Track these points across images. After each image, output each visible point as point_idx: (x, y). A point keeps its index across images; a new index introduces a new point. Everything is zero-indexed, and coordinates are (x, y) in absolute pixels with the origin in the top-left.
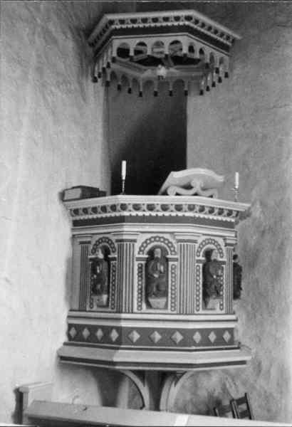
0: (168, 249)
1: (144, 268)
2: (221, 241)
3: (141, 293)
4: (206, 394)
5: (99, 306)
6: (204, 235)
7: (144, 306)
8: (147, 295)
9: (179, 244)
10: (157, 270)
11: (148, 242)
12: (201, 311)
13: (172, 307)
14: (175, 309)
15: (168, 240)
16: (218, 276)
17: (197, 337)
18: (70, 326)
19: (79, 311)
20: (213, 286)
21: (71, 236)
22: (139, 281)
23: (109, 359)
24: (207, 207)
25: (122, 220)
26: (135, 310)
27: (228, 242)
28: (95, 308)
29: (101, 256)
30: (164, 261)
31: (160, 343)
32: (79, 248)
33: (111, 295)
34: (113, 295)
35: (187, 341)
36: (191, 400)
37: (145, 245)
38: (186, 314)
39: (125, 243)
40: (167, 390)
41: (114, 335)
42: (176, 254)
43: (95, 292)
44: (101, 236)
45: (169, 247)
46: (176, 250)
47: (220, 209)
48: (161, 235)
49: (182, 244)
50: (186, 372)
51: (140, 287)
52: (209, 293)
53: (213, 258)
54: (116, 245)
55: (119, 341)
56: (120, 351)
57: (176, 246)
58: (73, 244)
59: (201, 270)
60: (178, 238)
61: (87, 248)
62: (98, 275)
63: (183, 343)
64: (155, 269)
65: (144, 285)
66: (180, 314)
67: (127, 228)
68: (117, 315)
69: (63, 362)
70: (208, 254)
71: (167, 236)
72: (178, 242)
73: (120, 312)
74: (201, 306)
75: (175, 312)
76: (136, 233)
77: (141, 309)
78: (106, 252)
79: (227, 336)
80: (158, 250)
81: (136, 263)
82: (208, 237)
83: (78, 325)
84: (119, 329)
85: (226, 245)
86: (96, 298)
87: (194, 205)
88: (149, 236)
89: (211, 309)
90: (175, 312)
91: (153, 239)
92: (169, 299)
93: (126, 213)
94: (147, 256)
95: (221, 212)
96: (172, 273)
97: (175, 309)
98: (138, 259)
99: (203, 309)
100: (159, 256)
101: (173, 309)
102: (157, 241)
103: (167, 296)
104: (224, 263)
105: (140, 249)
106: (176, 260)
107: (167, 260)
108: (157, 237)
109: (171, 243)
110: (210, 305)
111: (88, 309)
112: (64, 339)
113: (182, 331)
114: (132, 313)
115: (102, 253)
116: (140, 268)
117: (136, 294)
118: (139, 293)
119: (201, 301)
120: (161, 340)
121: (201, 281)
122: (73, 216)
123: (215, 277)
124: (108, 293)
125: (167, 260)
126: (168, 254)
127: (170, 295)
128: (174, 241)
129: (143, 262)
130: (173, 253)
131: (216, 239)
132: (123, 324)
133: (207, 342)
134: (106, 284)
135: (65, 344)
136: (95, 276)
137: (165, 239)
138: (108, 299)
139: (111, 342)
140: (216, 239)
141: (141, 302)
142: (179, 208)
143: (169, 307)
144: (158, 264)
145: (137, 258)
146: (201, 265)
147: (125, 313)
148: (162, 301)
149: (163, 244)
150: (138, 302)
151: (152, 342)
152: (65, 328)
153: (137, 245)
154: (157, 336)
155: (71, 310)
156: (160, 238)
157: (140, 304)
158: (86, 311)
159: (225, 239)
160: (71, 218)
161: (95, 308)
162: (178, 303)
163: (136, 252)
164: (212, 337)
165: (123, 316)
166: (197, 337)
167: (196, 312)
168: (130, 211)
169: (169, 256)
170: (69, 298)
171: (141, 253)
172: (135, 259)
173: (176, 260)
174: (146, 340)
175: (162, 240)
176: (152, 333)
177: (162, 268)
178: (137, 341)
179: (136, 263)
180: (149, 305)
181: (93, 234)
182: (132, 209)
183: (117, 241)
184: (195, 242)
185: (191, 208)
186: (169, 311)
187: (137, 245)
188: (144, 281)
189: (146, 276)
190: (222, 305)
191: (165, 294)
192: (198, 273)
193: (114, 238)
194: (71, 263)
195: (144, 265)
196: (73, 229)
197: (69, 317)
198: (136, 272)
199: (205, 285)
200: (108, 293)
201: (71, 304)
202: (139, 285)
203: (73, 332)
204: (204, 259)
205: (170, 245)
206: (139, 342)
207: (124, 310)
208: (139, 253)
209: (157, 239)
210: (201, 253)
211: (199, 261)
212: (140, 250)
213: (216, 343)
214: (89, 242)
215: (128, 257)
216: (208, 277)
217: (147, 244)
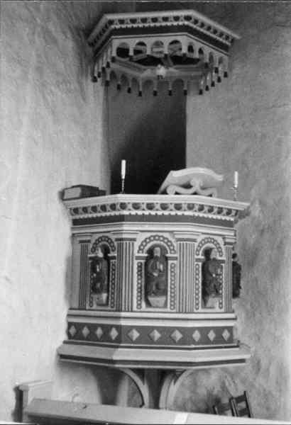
0: (167, 247)
1: (143, 267)
2: (220, 240)
3: (141, 292)
4: (205, 393)
5: (99, 305)
6: (203, 233)
7: (144, 304)
8: (147, 294)
9: (179, 242)
10: (156, 268)
11: (148, 240)
12: (200, 310)
13: (171, 305)
14: (174, 308)
15: (167, 239)
16: (217, 275)
17: (197, 335)
18: (70, 325)
19: (79, 309)
20: (212, 285)
21: (71, 235)
22: (138, 279)
23: (109, 358)
24: (206, 206)
25: (121, 219)
26: (135, 309)
27: (227, 240)
28: (95, 307)
29: (100, 255)
30: (164, 260)
31: (160, 341)
32: (79, 247)
33: (110, 293)
34: (113, 293)
35: (187, 339)
36: (191, 398)
37: (144, 244)
38: (186, 313)
39: (124, 242)
40: (167, 388)
41: (114, 333)
42: (175, 253)
43: (95, 290)
44: (101, 235)
45: (168, 246)
46: (175, 249)
47: (219, 208)
48: (160, 234)
49: (182, 242)
50: (185, 370)
51: (139, 286)
52: (208, 292)
53: (212, 257)
54: (116, 244)
55: (118, 340)
56: (120, 349)
57: (175, 244)
58: (73, 243)
59: (200, 269)
60: (177, 236)
61: (87, 247)
62: (98, 274)
63: (183, 341)
64: (155, 268)
65: (143, 284)
66: (179, 312)
67: (127, 227)
68: (117, 314)
69: (63, 360)
70: (207, 253)
71: (166, 235)
72: (177, 241)
73: (120, 310)
74: (200, 305)
75: (174, 311)
76: (136, 232)
77: (141, 307)
78: (106, 251)
80: (158, 249)
81: (136, 262)
82: (208, 236)
83: (78, 323)
84: (119, 328)
85: (225, 244)
86: (95, 296)
87: (193, 204)
88: (148, 235)
89: (210, 308)
90: (174, 311)
91: (152, 238)
92: (169, 297)
93: (125, 212)
94: (146, 255)
95: (220, 211)
96: (172, 272)
97: (174, 308)
98: (138, 258)
99: (202, 307)
100: (159, 255)
101: (172, 307)
102: (157, 240)
103: (167, 294)
104: (223, 262)
105: (139, 247)
106: (176, 259)
107: (167, 259)
108: (157, 236)
109: (170, 242)
110: (209, 304)
111: (87, 308)
112: (64, 337)
113: (181, 330)
114: (132, 311)
115: (102, 251)
116: (140, 267)
117: (135, 292)
118: (138, 292)
119: (200, 299)
120: (160, 338)
121: (200, 280)
122: (72, 215)
123: (214, 275)
124: (108, 291)
125: (167, 259)
126: (167, 253)
127: (169, 293)
128: (173, 240)
129: (143, 261)
130: (173, 252)
131: (216, 238)
132: (123, 323)
133: (207, 341)
134: (106, 283)
135: (65, 342)
136: (95, 275)
137: (164, 238)
138: (108, 298)
139: (111, 341)
140: (216, 238)
141: (140, 300)
142: (178, 207)
143: (169, 306)
144: (158, 263)
145: (136, 257)
146: (200, 264)
147: (125, 311)
148: (161, 300)
149: (162, 243)
150: (138, 300)
151: (151, 340)
152: (65, 326)
153: (137, 244)
154: (157, 335)
155: (71, 309)
156: (159, 237)
157: (139, 302)
158: (85, 309)
159: (224, 238)
160: (71, 217)
161: (95, 307)
162: (177, 302)
163: (136, 251)
164: (212, 335)
165: (123, 314)
166: (197, 335)
167: (195, 311)
168: (130, 210)
169: (168, 255)
170: (69, 297)
171: (141, 252)
172: (134, 258)
173: (176, 259)
174: (146, 338)
175: (161, 239)
176: (151, 332)
177: (161, 267)
178: (137, 339)
179: (136, 262)
180: (149, 304)
181: (93, 233)
182: (131, 208)
183: (117, 240)
184: (194, 240)
185: (191, 207)
186: (169, 310)
187: (137, 244)
188: (143, 279)
189: (146, 275)
190: (221, 303)
191: (165, 293)
192: (197, 272)
193: (113, 237)
194: (70, 261)
195: (143, 264)
196: (72, 228)
197: (69, 315)
198: (135, 270)
199: (204, 284)
200: (108, 291)
201: (70, 303)
202: (138, 283)
203: (73, 330)
204: (203, 257)
205: (169, 244)
206: (138, 341)
207: (123, 309)
208: (138, 252)
209: (157, 238)
210: (201, 252)
211: (198, 260)
212: (140, 249)
213: (216, 341)
214: (89, 241)
215: (128, 255)
216: (208, 275)
217: (147, 243)
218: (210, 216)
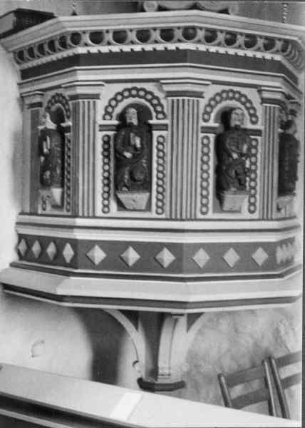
0: (152, 108)
1: (112, 143)
2: (252, 95)
4: (251, 342)
5: (55, 207)
6: (215, 82)
7: (113, 205)
8: (116, 188)
9: (170, 99)
10: (129, 143)
12: (210, 215)
13: (158, 207)
15: (151, 93)
16: (241, 155)
18: (21, 237)
19: (30, 214)
20: (233, 173)
21: (18, 95)
22: (105, 164)
23: (52, 292)
24: (222, 31)
25: (76, 60)
27: (266, 95)
28: (49, 210)
29: (51, 125)
30: (144, 129)
31: (137, 266)
32: (28, 113)
34: (69, 188)
35: (182, 266)
36: (229, 350)
37: (113, 103)
38: (182, 220)
41: (68, 252)
42: (165, 117)
43: (45, 184)
46: (165, 111)
47: (248, 36)
48: (139, 85)
49: (175, 98)
50: (199, 315)
52: (225, 186)
53: (234, 123)
55: (74, 264)
56: (73, 278)
57: (163, 102)
58: (22, 110)
59: (212, 146)
60: (166, 88)
61: (37, 112)
62: (46, 156)
63: (176, 266)
64: (127, 144)
65: (112, 171)
66: (171, 219)
67: (84, 75)
68: (69, 221)
69: (7, 291)
70: (225, 116)
71: (149, 87)
72: (167, 96)
73: (75, 216)
74: (210, 205)
80: (133, 111)
82: (129, 85)
83: (44, 237)
84: (75, 243)
85: (264, 101)
86: (44, 193)
87: (194, 28)
89: (231, 211)
90: (163, 216)
91: (243, 99)
92: (154, 193)
93: (81, 50)
94: (116, 122)
96: (159, 150)
98: (103, 128)
99: (214, 211)
100: (135, 122)
102: (134, 96)
103: (150, 190)
104: (258, 133)
106: (165, 127)
107: (151, 128)
108: (134, 88)
109: (157, 98)
110: (227, 205)
112: (13, 257)
113: (172, 247)
114: (94, 217)
115: (52, 120)
116: (106, 142)
118: (105, 185)
119: (211, 197)
120: (138, 261)
121: (211, 163)
122: (18, 63)
123: (235, 156)
124: (62, 186)
125: (151, 128)
127: (154, 187)
128: (161, 95)
129: (111, 133)
130: (161, 116)
131: (244, 91)
132: (80, 235)
134: (58, 171)
135: (13, 265)
136: (42, 159)
137: (147, 92)
138: (63, 193)
140: (244, 91)
141: (108, 199)
142: (167, 35)
143: (154, 207)
144: (132, 135)
145: (101, 126)
146: (212, 137)
147: (83, 217)
148: (141, 198)
149: (143, 101)
151: (124, 264)
152: (14, 239)
153: (101, 105)
154: (132, 256)
155: (22, 213)
156: (138, 90)
157: (106, 202)
159: (260, 91)
160: (18, 67)
162: (167, 201)
164: (98, 255)
165: (79, 222)
167: (199, 216)
169: (153, 121)
170: (17, 192)
173: (165, 127)
174: (115, 264)
177: (138, 142)
184: (200, 95)
185: (189, 34)
186: (154, 215)
187: (101, 105)
188: (112, 164)
189: (116, 157)
190: (251, 204)
191: (146, 186)
192: (206, 150)
194: (18, 138)
195: (112, 138)
196: (19, 84)
197: (18, 223)
198: (99, 149)
199: (218, 170)
201: (22, 204)
203: (23, 247)
204: (217, 125)
205: (155, 102)
206: (104, 265)
207: (81, 214)
208: (104, 119)
210: (213, 115)
211: (206, 130)
212: (107, 113)
216: (225, 156)
218: (250, 53)
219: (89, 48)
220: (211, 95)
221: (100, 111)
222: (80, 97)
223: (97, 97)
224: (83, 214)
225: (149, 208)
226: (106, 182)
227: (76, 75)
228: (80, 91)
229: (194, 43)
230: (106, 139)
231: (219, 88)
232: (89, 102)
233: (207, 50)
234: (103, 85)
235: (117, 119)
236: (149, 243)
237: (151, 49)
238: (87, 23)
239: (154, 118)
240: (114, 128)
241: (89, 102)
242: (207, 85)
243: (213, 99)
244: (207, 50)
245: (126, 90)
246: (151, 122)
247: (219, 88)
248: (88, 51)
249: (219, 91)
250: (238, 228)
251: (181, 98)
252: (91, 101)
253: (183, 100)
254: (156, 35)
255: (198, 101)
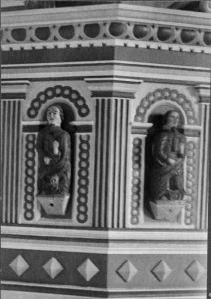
3: (138, 193)
6: (147, 80)
9: (95, 98)
10: (173, 150)
14: (191, 222)
26: (129, 225)
28: (38, 218)
33: (76, 195)
39: (113, 99)
44: (52, 84)
45: (182, 105)
48: (172, 87)
51: (136, 181)
54: (91, 103)
71: (182, 89)
75: (192, 227)
76: (135, 81)
77: (138, 222)
78: (67, 116)
79: (90, 270)
81: (131, 137)
82: (162, 86)
86: (46, 201)
90: (192, 227)
91: (50, 93)
94: (151, 125)
95: (163, 35)
97: (191, 222)
101: (188, 221)
102: (65, 96)
105: (138, 110)
106: (88, 129)
108: (167, 89)
111: (21, 220)
114: (125, 228)
116: (138, 146)
117: (129, 193)
123: (172, 161)
126: (73, 119)
129: (143, 137)
132: (112, 250)
136: (47, 161)
141: (137, 208)
143: (75, 213)
150: (133, 208)
153: (134, 104)
156: (170, 92)
157: (135, 212)
158: (16, 224)
163: (133, 113)
164: (54, 267)
165: (112, 234)
166: (20, 265)
168: (55, 39)
171: (140, 118)
172: (21, 130)
175: (67, 92)
176: (45, 262)
178: (92, 279)
179: (131, 137)
180: (150, 213)
181: (31, 80)
182: (83, 35)
183: (95, 94)
186: (183, 226)
187: (134, 104)
193: (85, 90)
200: (71, 192)
202: (134, 178)
208: (136, 120)
209: (167, 94)
212: (138, 113)
213: (61, 278)
214: (22, 96)
219: (33, 44)
220: (144, 95)
221: (133, 113)
222: (114, 94)
223: (131, 95)
224: (11, 222)
225: (68, 214)
226: (136, 189)
227: (112, 69)
228: (116, 87)
229: (121, 38)
230: (137, 142)
231: (154, 87)
232: (122, 101)
233: (68, 46)
234: (139, 83)
235: (149, 121)
236: (40, 251)
237: (101, 45)
238: (163, 17)
239: (77, 116)
240: (145, 131)
241: (122, 101)
242: (139, 83)
243: (37, 100)
244: (68, 46)
245: (49, 89)
246: (75, 123)
247: (154, 87)
248: (11, 49)
249: (43, 90)
250: (127, 238)
251: (12, 100)
252: (125, 100)
253: (9, 102)
254: (79, 31)
255: (128, 101)
